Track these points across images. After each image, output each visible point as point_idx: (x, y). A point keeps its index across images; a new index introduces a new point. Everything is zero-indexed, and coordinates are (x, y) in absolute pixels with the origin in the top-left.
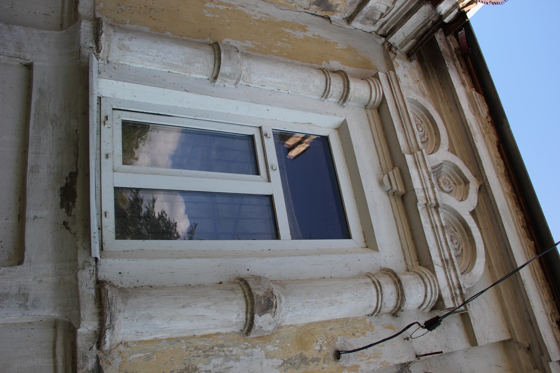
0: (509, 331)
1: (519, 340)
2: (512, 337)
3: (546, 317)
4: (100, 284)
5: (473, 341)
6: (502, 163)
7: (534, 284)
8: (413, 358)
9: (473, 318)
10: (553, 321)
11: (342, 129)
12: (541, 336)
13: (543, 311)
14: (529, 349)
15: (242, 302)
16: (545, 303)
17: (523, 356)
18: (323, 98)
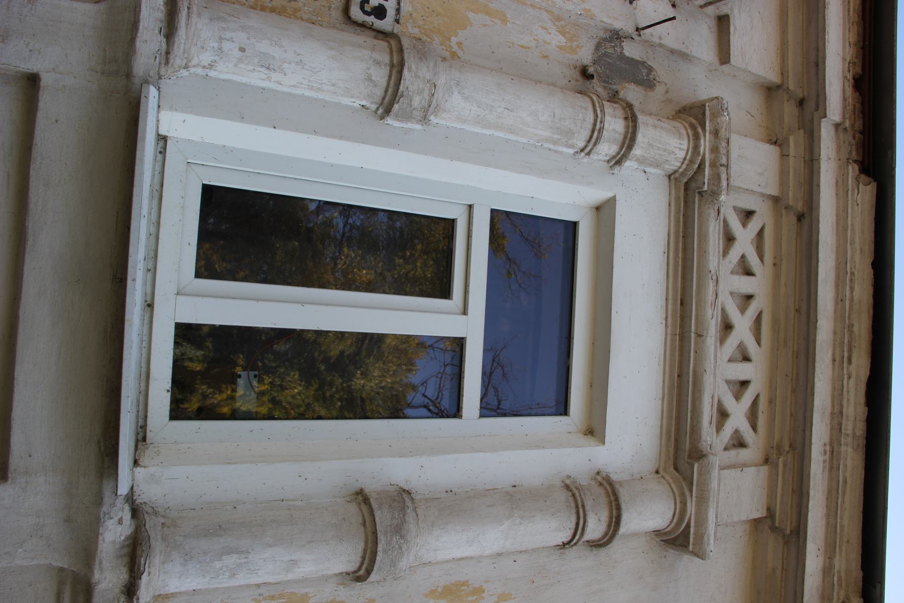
0: (782, 74)
1: (790, 88)
2: (783, 82)
3: (841, 63)
4: (163, 139)
5: (724, 55)
6: (871, 312)
7: (841, 15)
8: (631, 30)
9: (735, 28)
10: (849, 71)
11: (604, 211)
12: (824, 82)
13: (841, 53)
14: (801, 103)
15: (361, 546)
16: (847, 45)
17: (789, 110)
18: (583, 154)
